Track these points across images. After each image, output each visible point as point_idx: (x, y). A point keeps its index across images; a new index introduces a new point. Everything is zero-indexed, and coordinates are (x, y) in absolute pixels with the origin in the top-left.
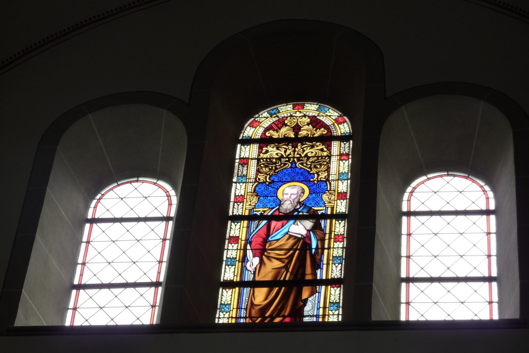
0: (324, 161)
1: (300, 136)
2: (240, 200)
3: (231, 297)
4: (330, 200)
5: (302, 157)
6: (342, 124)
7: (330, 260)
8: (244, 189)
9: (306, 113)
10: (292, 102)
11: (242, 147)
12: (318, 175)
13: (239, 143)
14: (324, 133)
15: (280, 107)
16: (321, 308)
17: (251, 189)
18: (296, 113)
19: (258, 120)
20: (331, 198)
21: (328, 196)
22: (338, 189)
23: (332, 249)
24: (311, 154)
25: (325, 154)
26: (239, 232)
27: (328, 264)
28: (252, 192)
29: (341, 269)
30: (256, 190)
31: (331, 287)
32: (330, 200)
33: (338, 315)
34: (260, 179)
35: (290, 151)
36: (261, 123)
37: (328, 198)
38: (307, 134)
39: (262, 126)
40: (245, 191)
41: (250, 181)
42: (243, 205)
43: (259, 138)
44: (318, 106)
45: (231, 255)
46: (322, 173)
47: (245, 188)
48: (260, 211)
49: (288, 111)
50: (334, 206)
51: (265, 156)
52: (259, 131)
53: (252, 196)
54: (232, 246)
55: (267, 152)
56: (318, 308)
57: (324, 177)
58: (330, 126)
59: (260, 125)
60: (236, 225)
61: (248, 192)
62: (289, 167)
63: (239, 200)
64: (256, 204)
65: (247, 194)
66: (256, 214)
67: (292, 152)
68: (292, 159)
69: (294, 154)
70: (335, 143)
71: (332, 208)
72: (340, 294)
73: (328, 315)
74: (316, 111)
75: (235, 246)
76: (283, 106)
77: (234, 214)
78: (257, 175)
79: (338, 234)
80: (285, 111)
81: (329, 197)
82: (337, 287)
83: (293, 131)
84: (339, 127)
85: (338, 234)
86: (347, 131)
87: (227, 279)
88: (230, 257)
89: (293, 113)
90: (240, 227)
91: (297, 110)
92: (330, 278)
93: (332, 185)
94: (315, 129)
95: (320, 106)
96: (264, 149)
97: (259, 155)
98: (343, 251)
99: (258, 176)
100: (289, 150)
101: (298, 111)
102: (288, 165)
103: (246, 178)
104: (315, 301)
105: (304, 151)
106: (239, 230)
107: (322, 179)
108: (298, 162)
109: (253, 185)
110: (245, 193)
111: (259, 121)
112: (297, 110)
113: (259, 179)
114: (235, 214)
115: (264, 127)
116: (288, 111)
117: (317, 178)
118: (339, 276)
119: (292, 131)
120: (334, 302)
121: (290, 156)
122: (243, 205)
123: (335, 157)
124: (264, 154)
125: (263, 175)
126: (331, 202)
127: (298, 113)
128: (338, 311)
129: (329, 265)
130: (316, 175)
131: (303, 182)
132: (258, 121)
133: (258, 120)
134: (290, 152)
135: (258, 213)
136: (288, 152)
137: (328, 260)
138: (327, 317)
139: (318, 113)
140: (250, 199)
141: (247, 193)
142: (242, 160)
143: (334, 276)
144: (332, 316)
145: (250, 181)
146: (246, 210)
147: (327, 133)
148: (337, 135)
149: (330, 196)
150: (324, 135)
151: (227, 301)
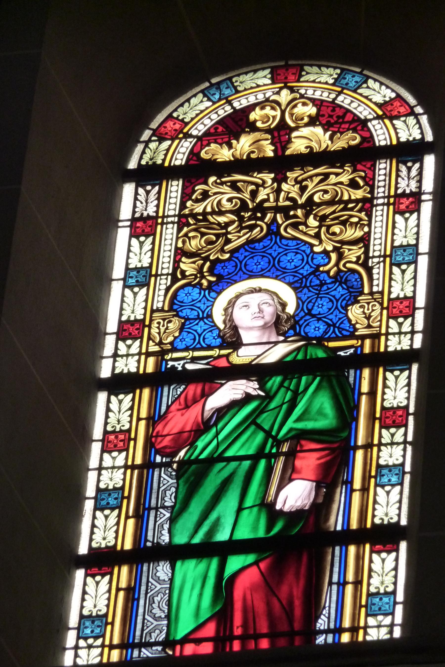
1: (288, 174)
2: (111, 503)
6: (403, 119)
9: (306, 90)
10: (267, 61)
13: (78, 567)
14: (353, 143)
15: (238, 75)
16: (356, 490)
17: (161, 298)
18: (278, 93)
19: (179, 116)
21: (362, 310)
23: (375, 449)
24: (323, 196)
25: (359, 194)
27: (365, 489)
28: (166, 308)
29: (409, 385)
30: (178, 298)
33: (392, 626)
34: (186, 271)
35: (268, 191)
36: (187, 124)
37: (364, 313)
38: (307, 147)
40: (145, 308)
43: (183, 163)
44: (338, 71)
45: (109, 482)
49: (258, 86)
51: (199, 208)
52: (182, 146)
54: (117, 402)
55: (205, 195)
57: (354, 259)
61: (155, 308)
63: (108, 503)
64: (176, 338)
66: (173, 367)
67: (272, 193)
69: (277, 200)
70: (382, 166)
72: (400, 502)
73: (366, 627)
74: (333, 84)
75: (120, 460)
76: (246, 73)
80: (252, 88)
81: (366, 311)
82: (389, 552)
83: (272, 144)
84: (393, 125)
86: (390, 515)
87: (92, 613)
88: (89, 613)
94: (329, 133)
95: (342, 70)
96: (196, 188)
97: (183, 206)
98: (405, 450)
99: (181, 264)
100: (265, 188)
102: (259, 229)
103: (120, 496)
105: (303, 189)
106: (129, 412)
107: (348, 265)
108: (283, 222)
111: (182, 120)
113: (183, 272)
114: (120, 370)
116: (258, 86)
117: (337, 264)
118: (395, 519)
119: (269, 142)
120: (382, 591)
121: (266, 205)
124: (197, 201)
125: (194, 263)
126: (371, 323)
127: (285, 92)
128: (390, 617)
130: (334, 256)
131: (282, 486)
132: (180, 118)
133: (179, 116)
134: (268, 195)
135: (179, 366)
136: (262, 195)
137: (366, 478)
138: (361, 632)
139: (339, 89)
140: (158, 328)
143: (377, 588)
144: (376, 629)
149: (368, 309)
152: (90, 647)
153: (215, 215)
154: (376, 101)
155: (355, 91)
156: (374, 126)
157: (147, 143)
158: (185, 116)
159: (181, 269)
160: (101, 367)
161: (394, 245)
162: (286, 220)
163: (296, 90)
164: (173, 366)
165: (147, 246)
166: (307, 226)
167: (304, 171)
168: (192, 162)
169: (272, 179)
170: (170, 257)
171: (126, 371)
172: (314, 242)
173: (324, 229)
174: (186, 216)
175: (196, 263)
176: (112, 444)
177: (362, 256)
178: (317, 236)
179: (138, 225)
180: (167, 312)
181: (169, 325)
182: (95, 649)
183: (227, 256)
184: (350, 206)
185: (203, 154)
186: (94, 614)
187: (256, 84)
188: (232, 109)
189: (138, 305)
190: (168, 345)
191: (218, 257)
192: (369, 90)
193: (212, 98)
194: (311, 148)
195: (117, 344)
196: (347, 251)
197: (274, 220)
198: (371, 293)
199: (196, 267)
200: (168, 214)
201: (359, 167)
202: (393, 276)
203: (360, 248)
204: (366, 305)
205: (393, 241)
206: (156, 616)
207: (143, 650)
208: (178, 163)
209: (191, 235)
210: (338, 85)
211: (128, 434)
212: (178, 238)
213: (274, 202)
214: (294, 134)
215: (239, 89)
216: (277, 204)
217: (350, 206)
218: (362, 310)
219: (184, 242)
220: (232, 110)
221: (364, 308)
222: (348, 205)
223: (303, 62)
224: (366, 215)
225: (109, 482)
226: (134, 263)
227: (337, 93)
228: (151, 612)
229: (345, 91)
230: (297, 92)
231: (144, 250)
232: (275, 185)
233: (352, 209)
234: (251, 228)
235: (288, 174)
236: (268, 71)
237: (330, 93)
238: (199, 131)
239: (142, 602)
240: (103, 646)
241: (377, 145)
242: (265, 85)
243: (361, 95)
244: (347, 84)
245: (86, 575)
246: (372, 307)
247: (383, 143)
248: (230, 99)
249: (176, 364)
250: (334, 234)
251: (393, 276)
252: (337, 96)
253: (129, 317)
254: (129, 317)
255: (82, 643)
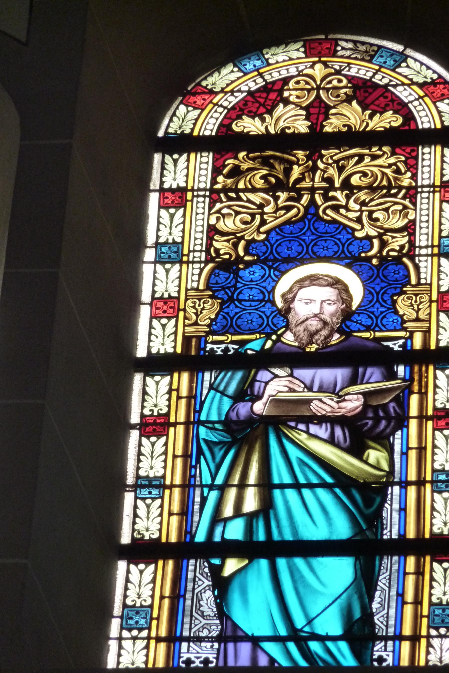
0: (395, 203)
3: (145, 651)
4: (417, 313)
5: (335, 190)
7: (422, 616)
8: (186, 170)
11: (132, 567)
12: (383, 244)
17: (196, 278)
18: (312, 67)
19: (207, 85)
20: (419, 305)
22: (441, 283)
23: (423, 641)
26: (163, 464)
28: (201, 287)
31: (435, 369)
32: (417, 313)
34: (219, 249)
39: (219, 104)
40: (179, 286)
41: (194, 257)
42: (176, 326)
45: (137, 599)
46: (393, 237)
47: (180, 278)
48: (222, 342)
49: (291, 59)
50: (429, 328)
53: (200, 300)
56: (404, 451)
58: (410, 105)
59: (215, 101)
60: (141, 572)
61: (189, 287)
62: (300, 215)
64: (212, 320)
65: (186, 296)
67: (307, 171)
68: (305, 199)
71: (427, 333)
77: (154, 351)
78: (210, 239)
79: (444, 468)
81: (413, 303)
84: (436, 107)
85: (444, 468)
89: (306, 68)
90: (166, 450)
91: (317, 59)
92: (433, 346)
93: (422, 270)
94: (368, 112)
96: (227, 163)
97: (214, 182)
101: (320, 61)
104: (389, 588)
106: (152, 585)
108: (323, 204)
109: (202, 270)
110: (179, 292)
112: (317, 59)
113: (217, 251)
115: (225, 108)
117: (381, 250)
119: (304, 117)
122: (176, 326)
123: (426, 261)
127: (318, 66)
129: (424, 451)
130: (376, 242)
133: (207, 85)
135: (219, 349)
139: (377, 68)
140: (194, 307)
141: (187, 290)
142: (166, 195)
145: (194, 257)
146: (179, 401)
147: (403, 125)
148: (433, 127)
150: (371, 645)
151: (149, 532)
152: (134, 638)
153: (248, 192)
154: (418, 81)
155: (393, 70)
156: (415, 107)
157: (192, 201)
158: (213, 86)
159: (214, 247)
160: (140, 318)
161: (442, 235)
162: (326, 201)
163: (331, 66)
164: (212, 349)
165: (178, 218)
166: (348, 210)
167: (340, 150)
168: (219, 134)
169: (306, 156)
170: (202, 226)
171: (162, 351)
172: (357, 226)
173: (365, 214)
174: (218, 192)
175: (231, 242)
176: (161, 310)
177: (407, 245)
178: (359, 220)
179: (164, 250)
180: (202, 291)
181: (205, 305)
182: (141, 641)
183: (263, 237)
184: (393, 191)
185: (234, 127)
186: (138, 605)
187: (289, 57)
188: (263, 82)
189: (172, 282)
190: (205, 327)
191: (254, 238)
192: (409, 69)
193: (243, 69)
194: (349, 127)
195: (145, 380)
196: (390, 238)
197: (312, 202)
198: (418, 284)
199: (231, 245)
200: (198, 187)
201: (398, 150)
202: (441, 268)
203: (403, 236)
204: (414, 298)
205: (440, 231)
206: (205, 614)
207: (191, 644)
208: (207, 133)
209: (225, 211)
210: (375, 63)
211: (163, 479)
212: (209, 214)
213: (310, 182)
214: (333, 111)
215: (270, 61)
216: (313, 185)
217: (393, 191)
218: (410, 301)
219: (218, 219)
220: (264, 83)
221: (412, 300)
222: (391, 190)
223: (339, 36)
224: (411, 202)
225: (154, 408)
226: (160, 290)
227: (375, 71)
228: (199, 609)
229: (383, 70)
230: (332, 68)
231: (175, 223)
232: (310, 162)
233: (395, 196)
234: (288, 209)
235: (323, 152)
236: (301, 43)
237: (367, 71)
238: (230, 103)
239: (188, 600)
240: (149, 638)
241: (420, 127)
242: (298, 58)
243: (400, 74)
244: (385, 62)
245: (141, 436)
246: (420, 299)
247: (426, 126)
248: (261, 71)
249: (215, 347)
250: (377, 220)
251: (441, 268)
252: (375, 74)
253: (163, 294)
254: (163, 294)
255: (125, 634)
